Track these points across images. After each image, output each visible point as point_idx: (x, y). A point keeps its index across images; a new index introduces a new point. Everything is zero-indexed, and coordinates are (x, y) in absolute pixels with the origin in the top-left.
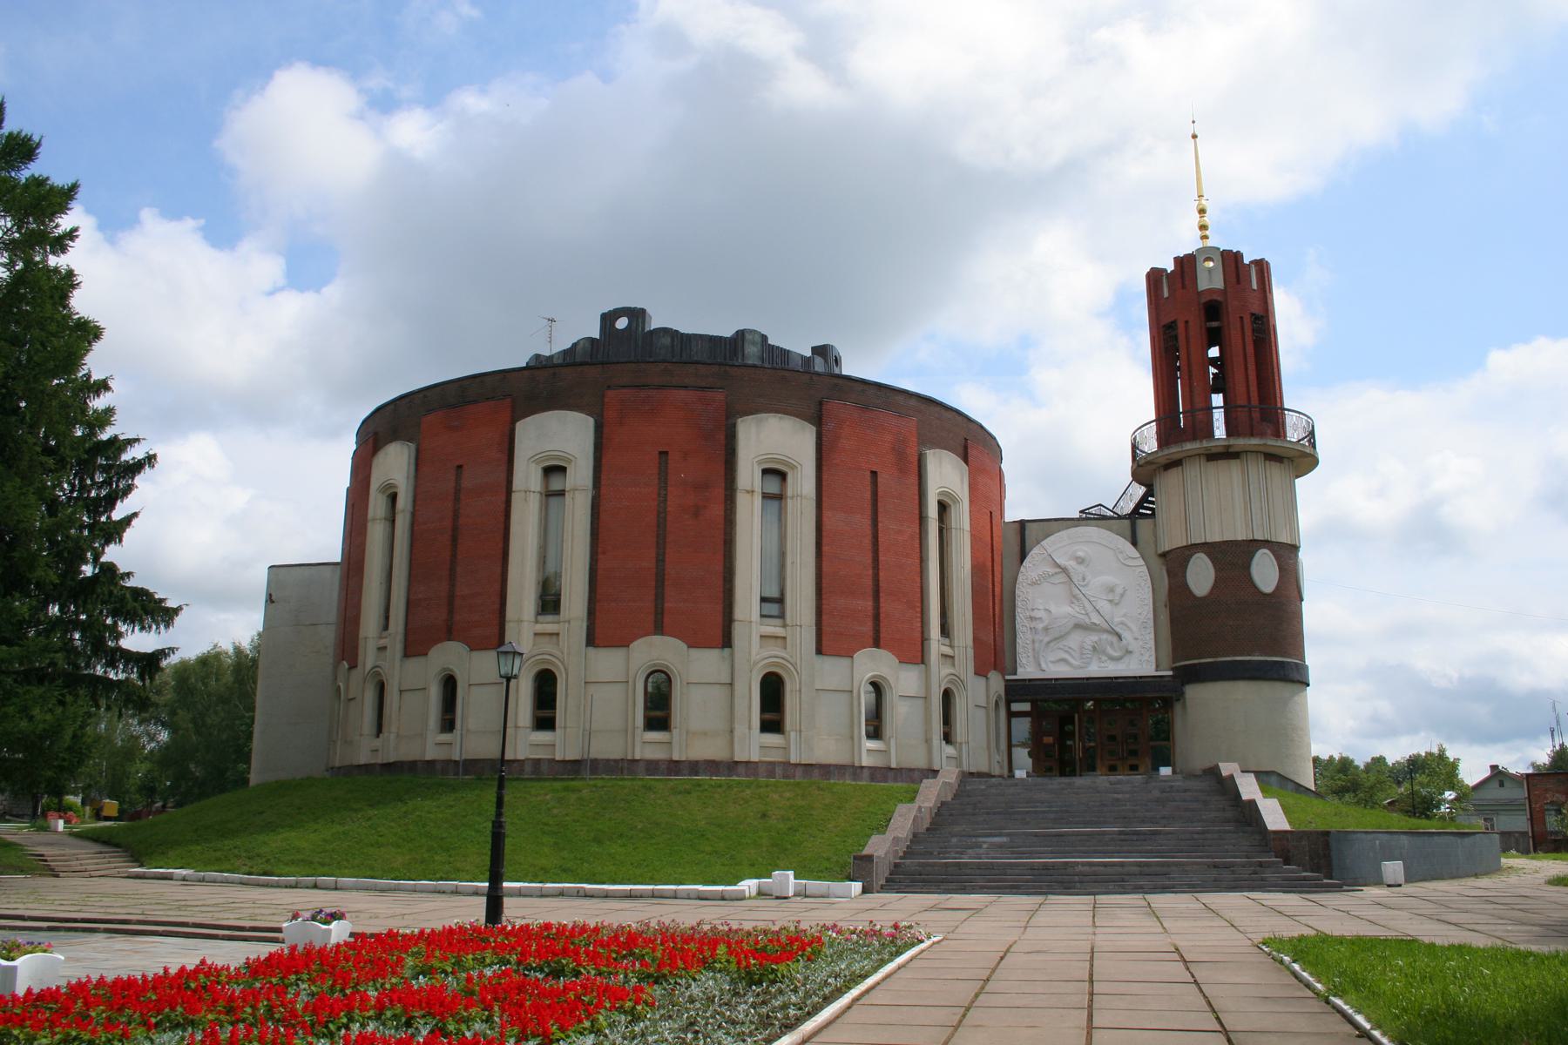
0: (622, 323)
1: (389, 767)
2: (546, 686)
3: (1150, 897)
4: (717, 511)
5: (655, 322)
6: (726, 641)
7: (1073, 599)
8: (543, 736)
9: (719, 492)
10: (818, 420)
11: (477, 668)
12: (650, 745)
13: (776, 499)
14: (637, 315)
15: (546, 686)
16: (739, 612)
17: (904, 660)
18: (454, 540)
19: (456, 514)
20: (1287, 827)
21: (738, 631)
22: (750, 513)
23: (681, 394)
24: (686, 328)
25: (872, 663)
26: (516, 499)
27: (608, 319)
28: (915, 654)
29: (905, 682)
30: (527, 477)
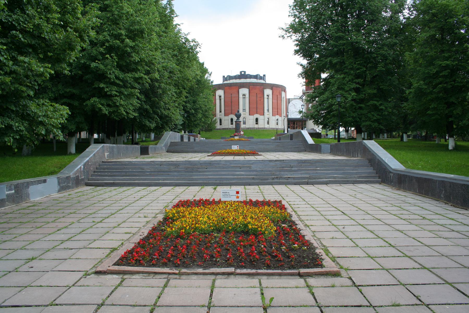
0: (243, 73)
1: (223, 129)
2: (221, 120)
3: (261, 187)
4: (262, 100)
5: (247, 73)
6: (264, 115)
7: (295, 108)
8: (221, 126)
9: (262, 98)
10: (272, 89)
11: (260, 118)
12: (256, 126)
13: (268, 98)
14: (245, 72)
15: (221, 120)
16: (265, 112)
17: (261, 115)
18: (231, 103)
19: (231, 100)
20: (314, 143)
21: (265, 114)
22: (266, 100)
23: (258, 87)
24: (251, 74)
25: (277, 117)
26: (240, 99)
27: (241, 72)
28: (281, 116)
29: (280, 119)
30: (241, 96)
